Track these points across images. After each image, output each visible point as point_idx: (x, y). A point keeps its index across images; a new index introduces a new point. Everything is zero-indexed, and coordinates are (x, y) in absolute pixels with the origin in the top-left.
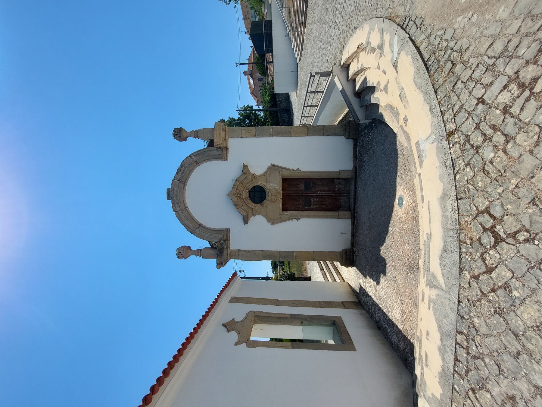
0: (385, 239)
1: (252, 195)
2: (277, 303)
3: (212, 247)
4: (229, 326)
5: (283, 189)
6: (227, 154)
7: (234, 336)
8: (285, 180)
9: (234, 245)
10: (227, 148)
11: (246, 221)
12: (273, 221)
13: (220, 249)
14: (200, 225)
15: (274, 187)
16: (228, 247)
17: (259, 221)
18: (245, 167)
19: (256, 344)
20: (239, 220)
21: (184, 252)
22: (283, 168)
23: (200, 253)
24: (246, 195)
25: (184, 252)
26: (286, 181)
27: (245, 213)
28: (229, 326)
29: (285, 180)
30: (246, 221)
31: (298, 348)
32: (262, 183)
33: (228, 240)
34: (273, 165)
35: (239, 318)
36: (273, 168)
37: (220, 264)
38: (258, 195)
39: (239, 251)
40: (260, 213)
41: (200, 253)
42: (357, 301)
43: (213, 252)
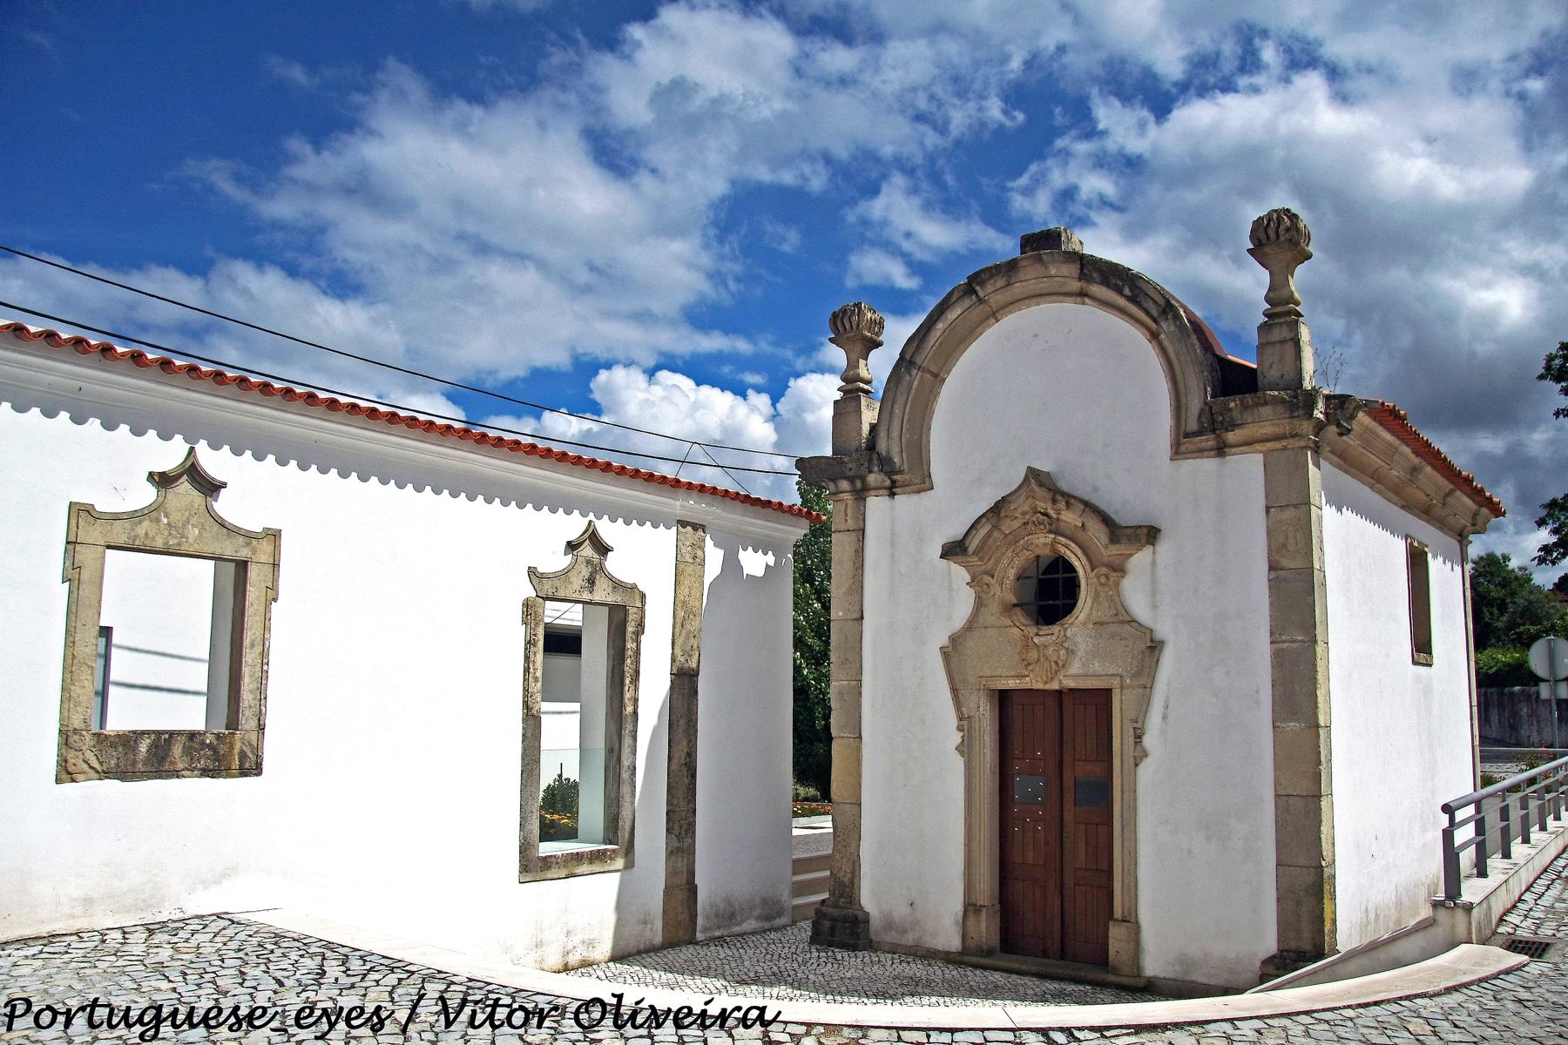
8: (1101, 699)
11: (953, 550)
29: (1101, 699)
30: (953, 550)
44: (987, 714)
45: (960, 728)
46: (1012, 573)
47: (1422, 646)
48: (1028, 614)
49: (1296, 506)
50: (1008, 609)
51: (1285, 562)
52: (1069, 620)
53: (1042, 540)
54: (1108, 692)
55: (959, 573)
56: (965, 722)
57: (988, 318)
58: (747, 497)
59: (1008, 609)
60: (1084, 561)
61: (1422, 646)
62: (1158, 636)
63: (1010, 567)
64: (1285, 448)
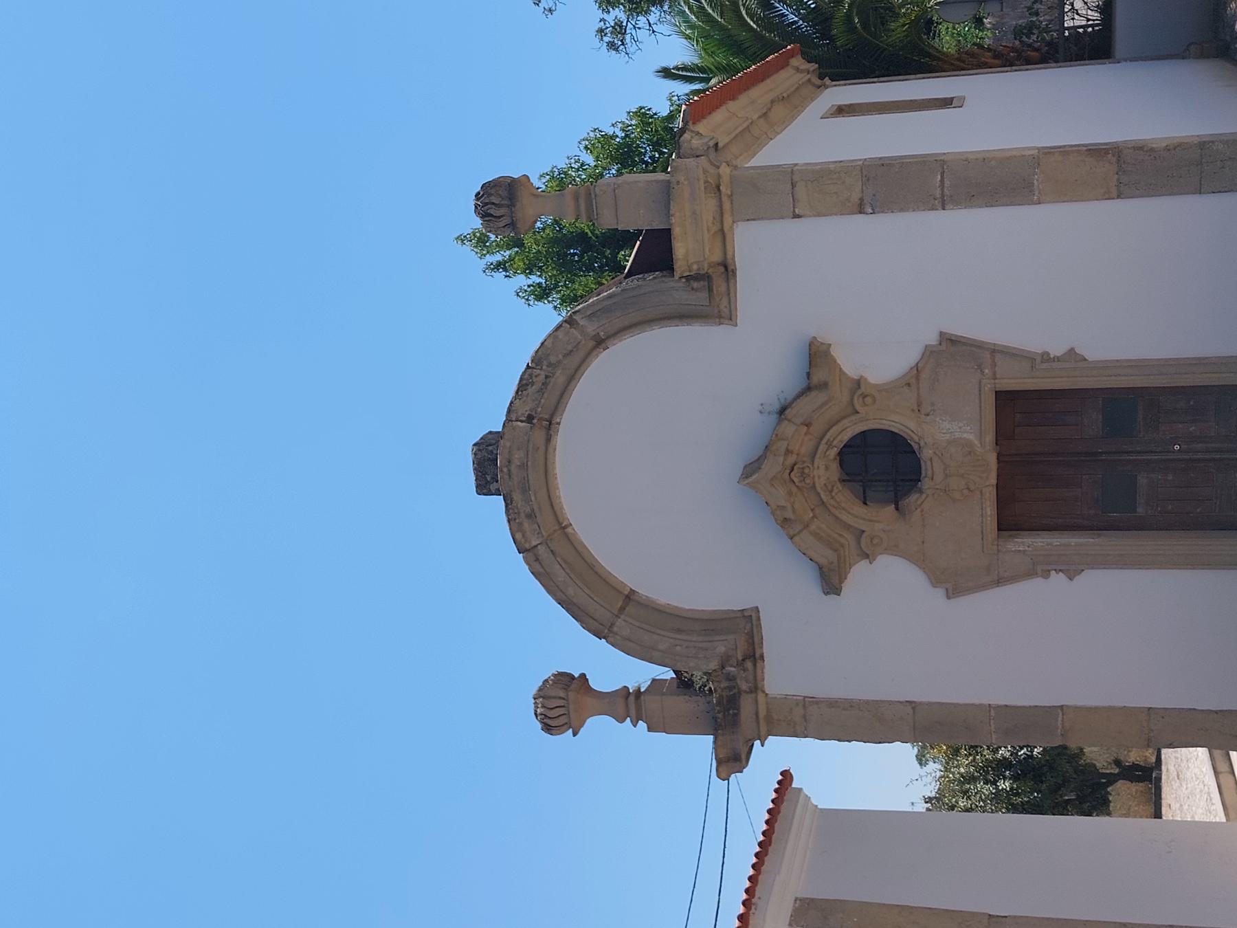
1: (853, 467)
6: (730, 294)
8: (1006, 400)
9: (782, 676)
10: (728, 269)
11: (831, 581)
12: (954, 583)
14: (630, 597)
15: (956, 434)
16: (756, 688)
20: (805, 581)
21: (564, 702)
23: (628, 705)
24: (825, 471)
25: (564, 702)
27: (825, 555)
29: (1006, 400)
30: (831, 581)
32: (899, 421)
33: (753, 656)
36: (951, 349)
38: (882, 466)
41: (628, 705)
43: (683, 704)
44: (1028, 541)
45: (1046, 574)
46: (859, 509)
47: (946, 103)
48: (907, 494)
49: (793, 185)
50: (921, 492)
51: (856, 196)
52: (913, 439)
53: (822, 471)
54: (998, 394)
55: (860, 576)
56: (1037, 568)
57: (566, 535)
58: (745, 903)
59: (921, 492)
60: (846, 422)
61: (946, 103)
62: (932, 339)
63: (853, 511)
64: (730, 196)
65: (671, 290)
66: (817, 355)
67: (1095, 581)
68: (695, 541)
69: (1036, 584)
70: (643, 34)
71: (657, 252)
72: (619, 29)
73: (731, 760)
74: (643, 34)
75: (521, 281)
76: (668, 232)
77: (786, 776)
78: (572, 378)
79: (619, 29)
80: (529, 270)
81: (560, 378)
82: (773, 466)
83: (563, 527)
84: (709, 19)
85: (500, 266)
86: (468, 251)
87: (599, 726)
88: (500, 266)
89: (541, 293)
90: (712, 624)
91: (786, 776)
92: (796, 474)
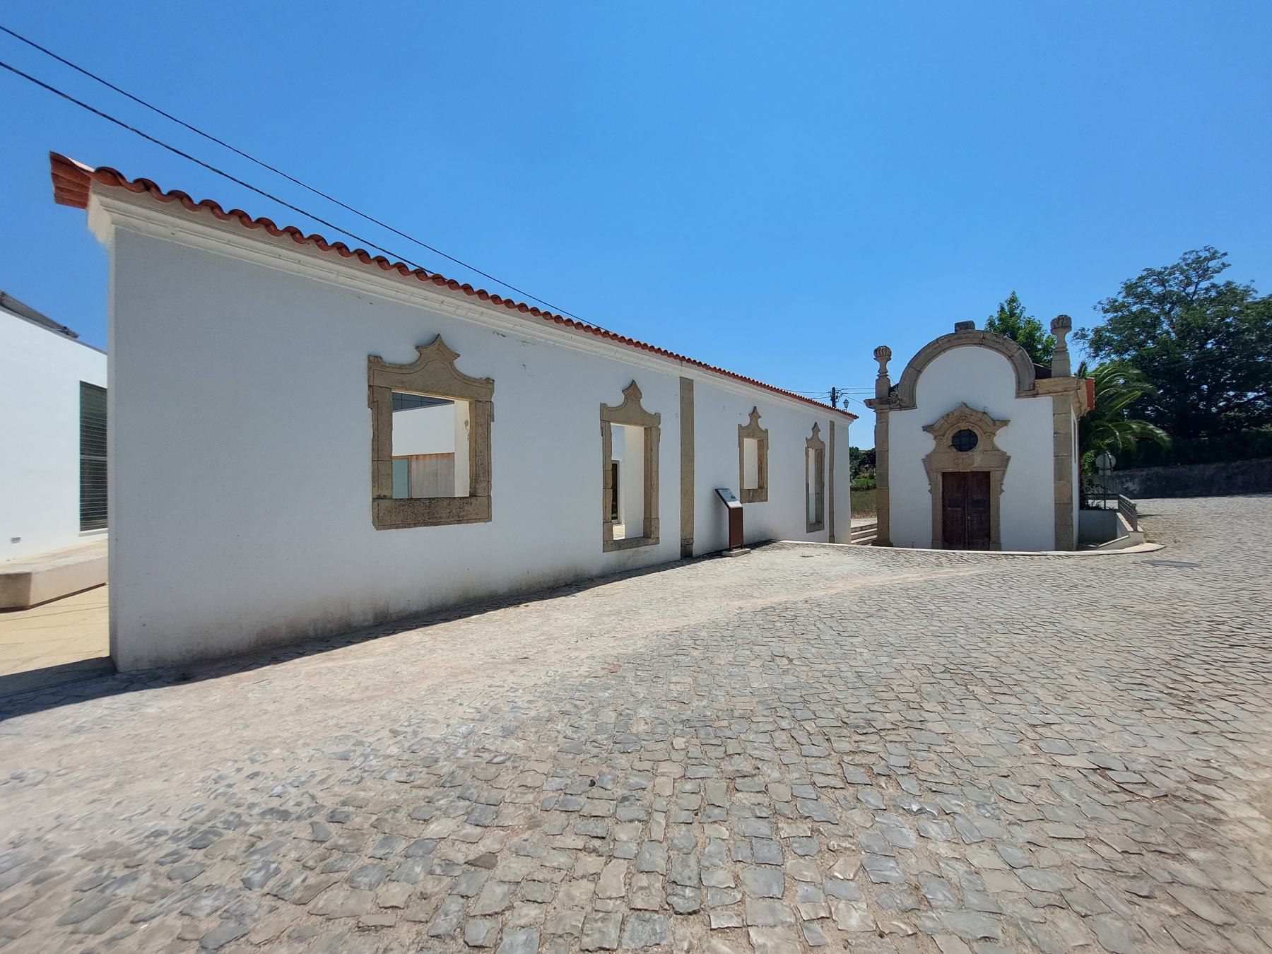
0: (485, 611)
1: (963, 433)
2: (831, 470)
3: (892, 389)
4: (632, 391)
5: (974, 473)
6: (1027, 396)
7: (617, 399)
8: (987, 475)
9: (894, 416)
10: (1035, 395)
11: (926, 428)
12: (927, 461)
13: (889, 399)
14: (920, 372)
15: (976, 460)
16: (891, 409)
17: (928, 444)
18: (1005, 422)
19: (741, 445)
20: (928, 420)
21: (883, 354)
22: (1004, 472)
23: (883, 374)
24: (964, 426)
25: (883, 354)
26: (983, 479)
27: (936, 427)
28: (632, 391)
29: (987, 475)
30: (926, 428)
31: (81, 440)
32: (981, 445)
33: (901, 408)
34: (1009, 458)
35: (648, 404)
36: (1005, 460)
37: (869, 403)
38: (965, 441)
39: (887, 423)
40: (937, 444)
41: (883, 374)
42: (694, 553)
43: (885, 392)
55: (931, 436)
65: (1029, 377)
66: (1005, 422)
67: (929, 497)
68: (939, 392)
69: (927, 481)
70: (1081, 346)
71: (1043, 373)
72: (1084, 336)
73: (869, 403)
74: (1081, 346)
75: (996, 315)
76: (1050, 376)
77: (856, 417)
78: (997, 350)
79: (1084, 336)
80: (1000, 320)
81: (997, 346)
82: (967, 411)
83: (944, 351)
84: (1104, 378)
85: (1002, 309)
86: (1008, 296)
87: (877, 365)
88: (1002, 309)
89: (991, 324)
90: (912, 396)
91: (856, 417)
92: (962, 417)
